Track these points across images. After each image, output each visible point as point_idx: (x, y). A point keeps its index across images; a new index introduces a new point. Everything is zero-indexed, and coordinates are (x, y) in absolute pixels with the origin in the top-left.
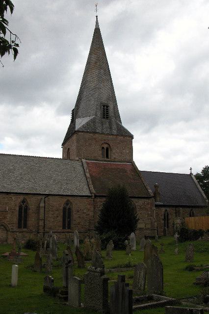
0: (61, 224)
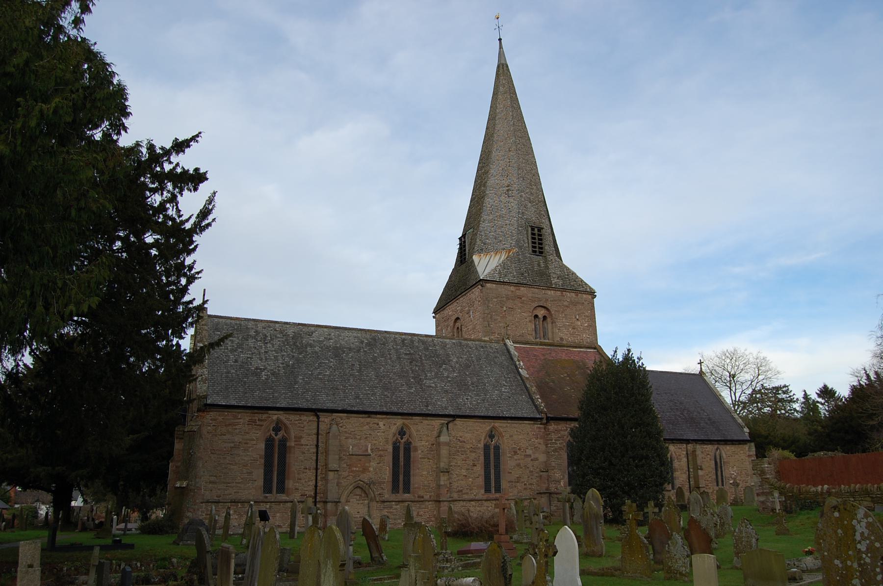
0: (481, 481)
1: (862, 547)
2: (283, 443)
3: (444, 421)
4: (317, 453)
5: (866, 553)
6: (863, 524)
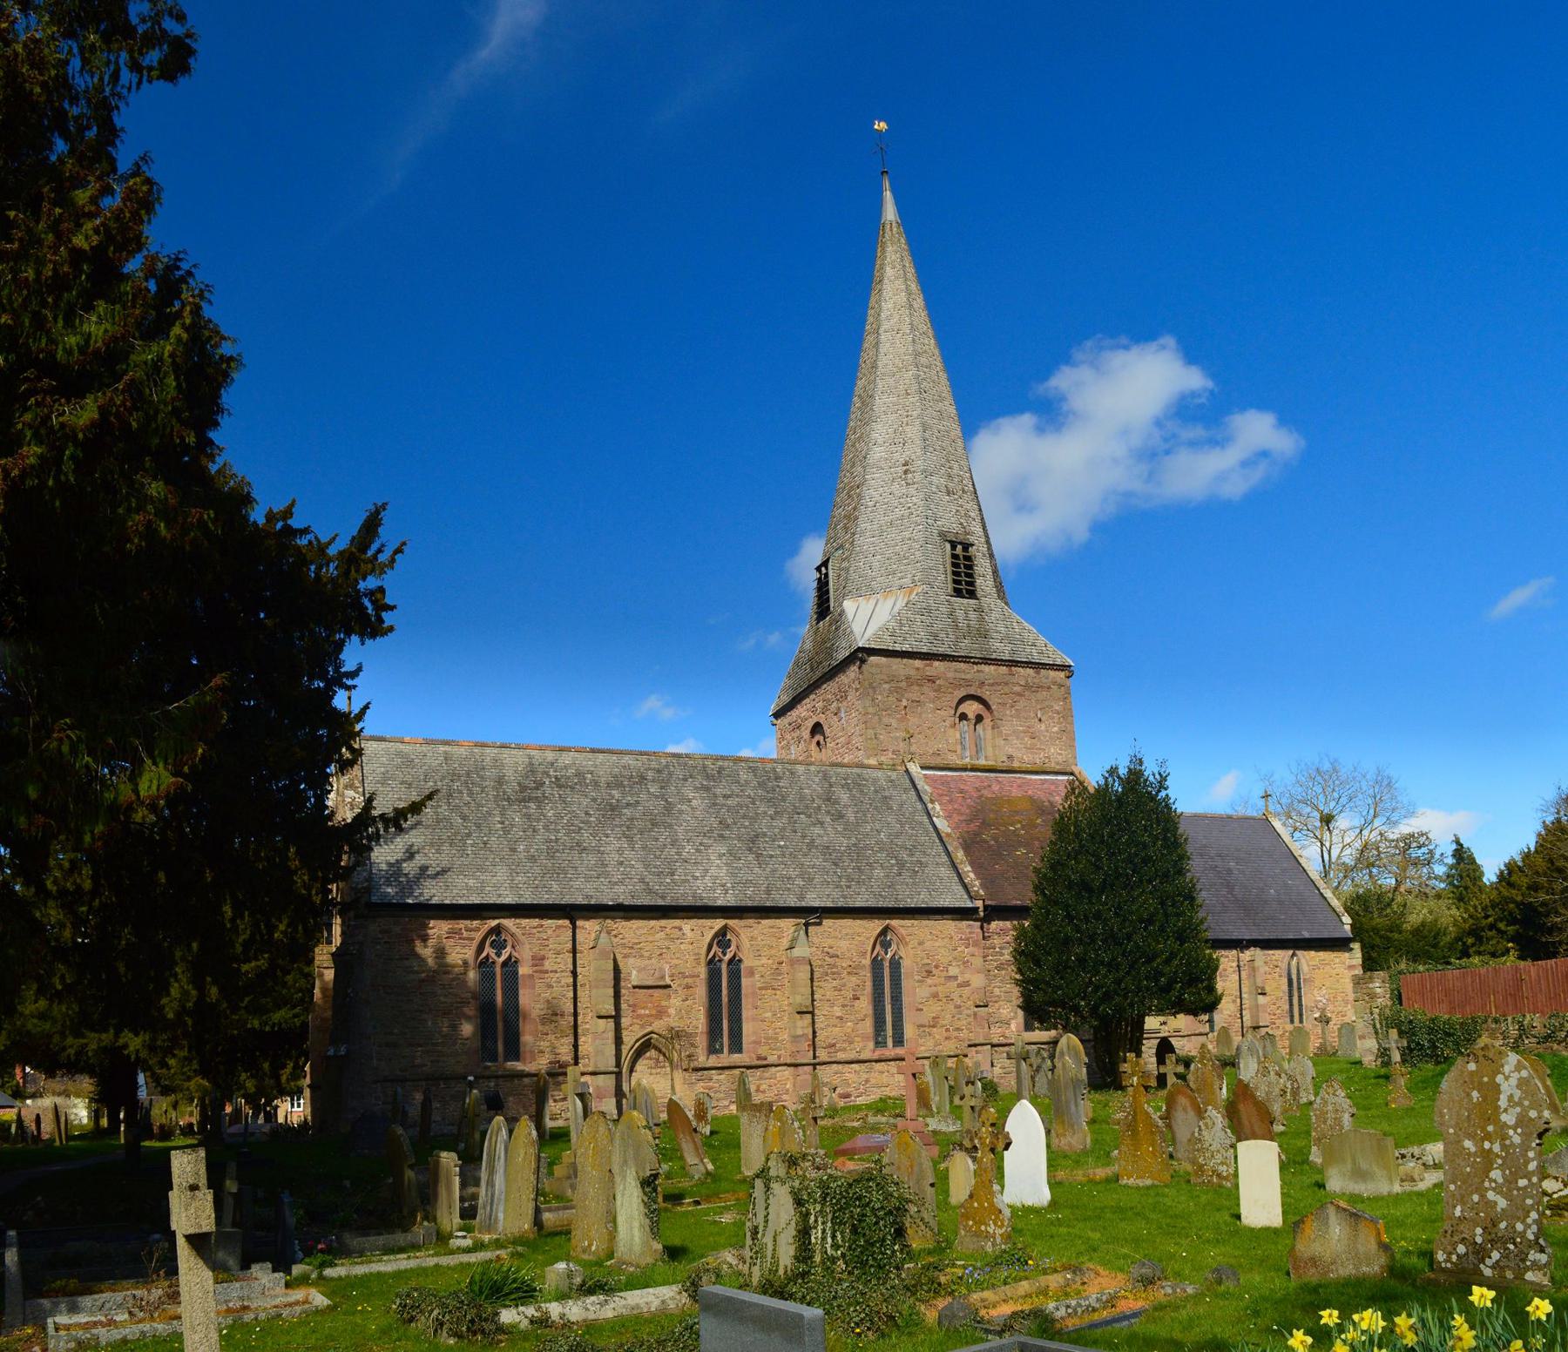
0: (868, 1026)
1: (1508, 1118)
4: (575, 986)
5: (1515, 1128)
6: (1513, 1081)
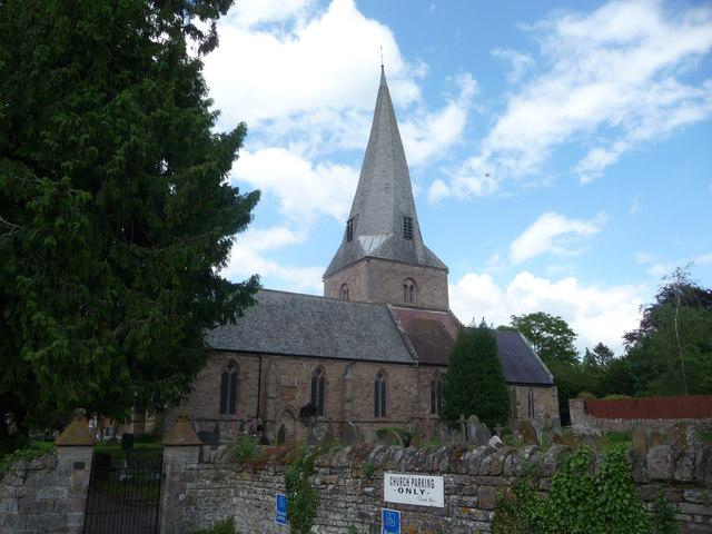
0: (372, 408)
2: (235, 375)
3: (349, 364)
